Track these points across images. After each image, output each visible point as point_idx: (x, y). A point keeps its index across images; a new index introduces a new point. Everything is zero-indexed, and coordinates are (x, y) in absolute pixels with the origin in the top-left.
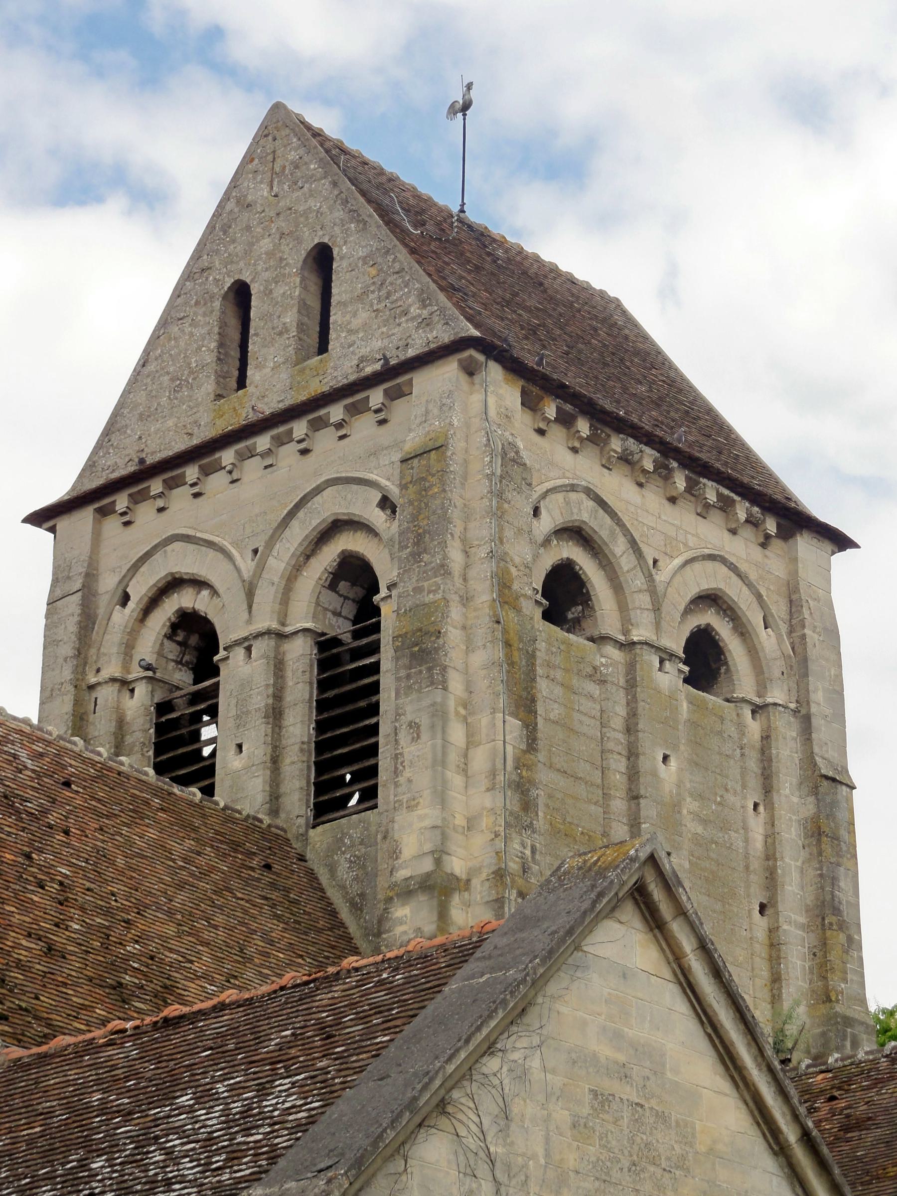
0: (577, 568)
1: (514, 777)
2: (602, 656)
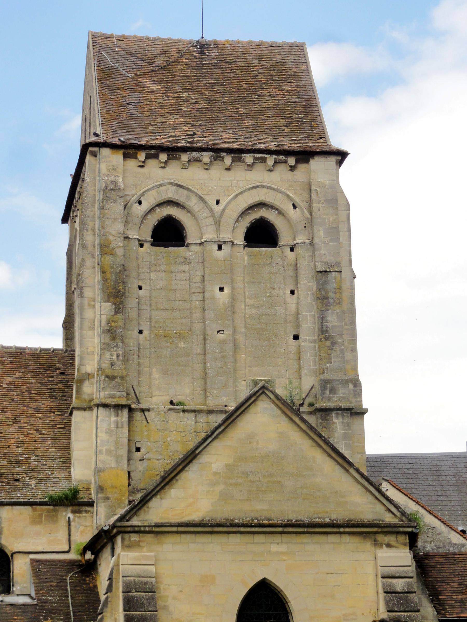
0: (174, 217)
1: (107, 328)
2: (190, 252)
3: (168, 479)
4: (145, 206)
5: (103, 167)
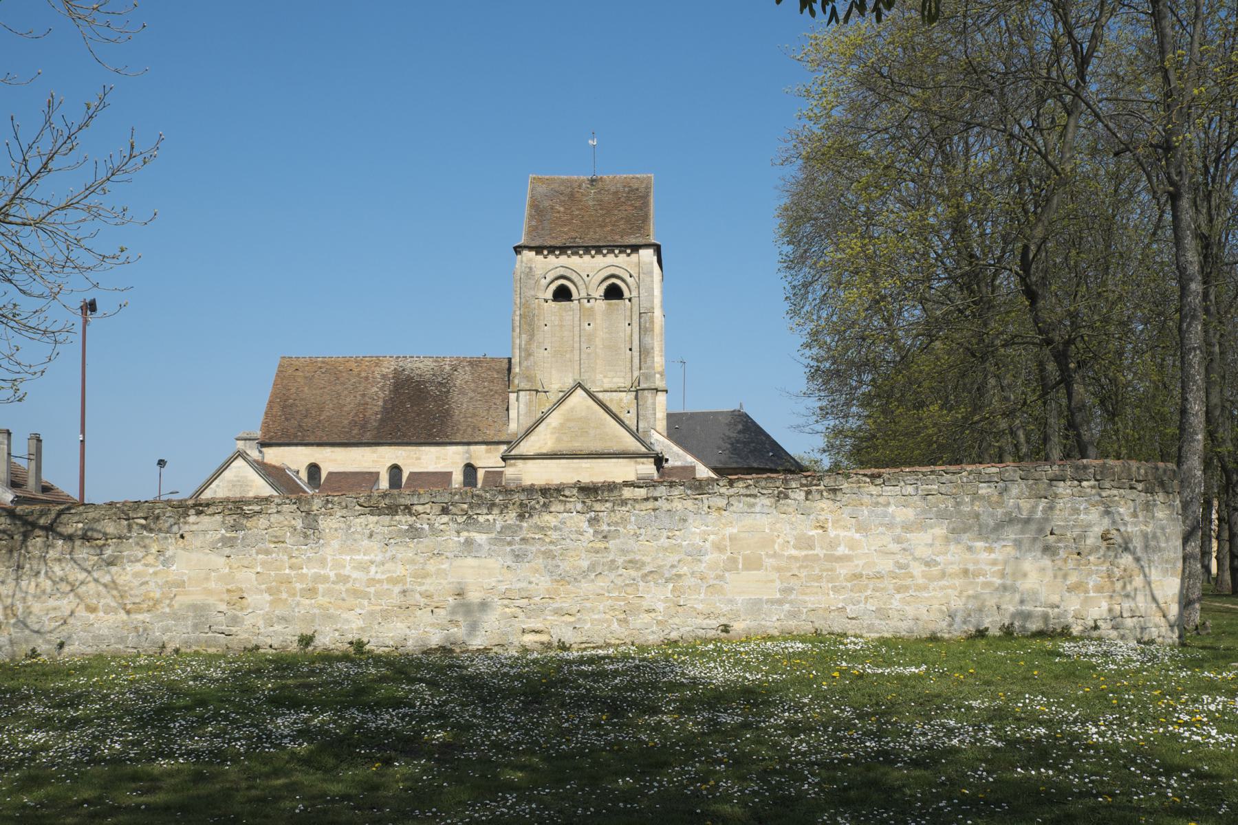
3: (529, 432)
4: (548, 280)
5: (524, 259)
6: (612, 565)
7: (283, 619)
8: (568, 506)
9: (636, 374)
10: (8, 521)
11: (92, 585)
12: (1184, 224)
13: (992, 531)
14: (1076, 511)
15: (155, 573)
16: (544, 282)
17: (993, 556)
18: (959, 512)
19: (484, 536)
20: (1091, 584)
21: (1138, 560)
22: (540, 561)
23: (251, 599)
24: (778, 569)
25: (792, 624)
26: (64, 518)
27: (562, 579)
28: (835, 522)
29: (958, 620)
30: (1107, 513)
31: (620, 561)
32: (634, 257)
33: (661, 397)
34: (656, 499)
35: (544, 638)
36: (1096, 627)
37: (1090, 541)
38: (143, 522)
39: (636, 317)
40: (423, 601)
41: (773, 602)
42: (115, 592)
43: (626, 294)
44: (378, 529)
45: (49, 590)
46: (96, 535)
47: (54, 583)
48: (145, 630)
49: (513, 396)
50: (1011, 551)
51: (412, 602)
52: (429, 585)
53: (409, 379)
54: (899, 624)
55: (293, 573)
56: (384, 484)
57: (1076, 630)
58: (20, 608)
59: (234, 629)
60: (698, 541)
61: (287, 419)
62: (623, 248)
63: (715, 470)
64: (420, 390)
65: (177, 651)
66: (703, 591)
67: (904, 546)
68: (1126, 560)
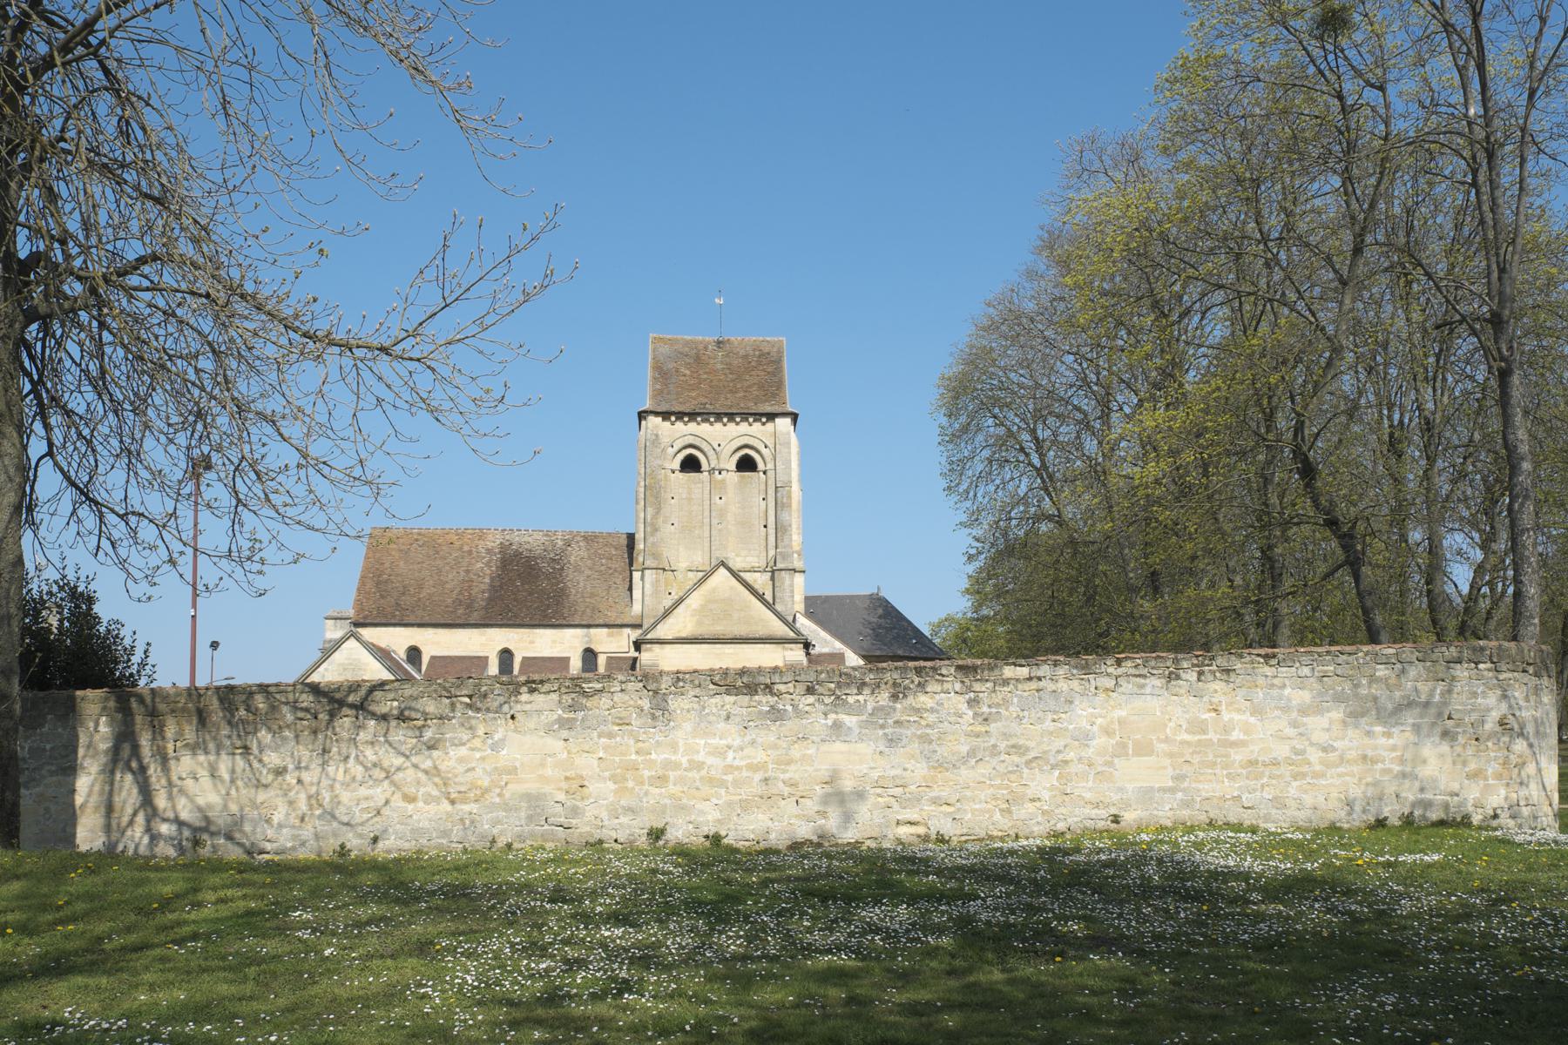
3: (667, 613)
6: (994, 751)
7: (630, 810)
8: (946, 686)
9: (772, 553)
10: (311, 698)
11: (411, 771)
12: (1513, 401)
13: (1390, 715)
14: (1475, 695)
15: (483, 759)
16: (671, 451)
17: (1391, 741)
18: (1356, 695)
19: (854, 719)
20: (1490, 771)
21: (1531, 746)
22: (915, 746)
23: (593, 787)
24: (1171, 755)
25: (1185, 814)
26: (378, 694)
27: (940, 766)
28: (1230, 704)
29: (1358, 808)
30: (1505, 697)
31: (1002, 746)
32: (770, 426)
33: (799, 579)
34: (1039, 679)
35: (921, 830)
36: (1495, 816)
37: (1488, 726)
38: (467, 700)
39: (771, 491)
40: (786, 790)
41: (1164, 790)
42: (437, 780)
43: (761, 466)
44: (736, 710)
45: (359, 778)
46: (414, 715)
47: (367, 769)
48: (472, 822)
49: (637, 575)
50: (1410, 736)
51: (775, 791)
52: (792, 773)
53: (518, 554)
54: (1297, 813)
55: (640, 759)
56: (493, 669)
57: (1476, 819)
58: (326, 796)
59: (574, 821)
60: (1084, 724)
61: (382, 597)
62: (758, 416)
63: (864, 657)
64: (531, 567)
65: (509, 846)
66: (1091, 777)
67: (1301, 730)
68: (1520, 746)
